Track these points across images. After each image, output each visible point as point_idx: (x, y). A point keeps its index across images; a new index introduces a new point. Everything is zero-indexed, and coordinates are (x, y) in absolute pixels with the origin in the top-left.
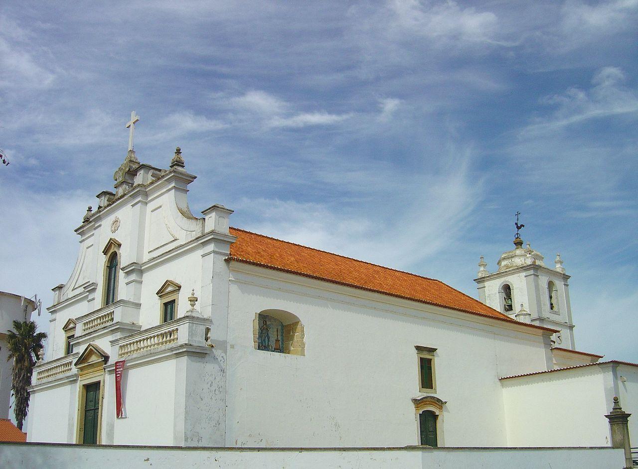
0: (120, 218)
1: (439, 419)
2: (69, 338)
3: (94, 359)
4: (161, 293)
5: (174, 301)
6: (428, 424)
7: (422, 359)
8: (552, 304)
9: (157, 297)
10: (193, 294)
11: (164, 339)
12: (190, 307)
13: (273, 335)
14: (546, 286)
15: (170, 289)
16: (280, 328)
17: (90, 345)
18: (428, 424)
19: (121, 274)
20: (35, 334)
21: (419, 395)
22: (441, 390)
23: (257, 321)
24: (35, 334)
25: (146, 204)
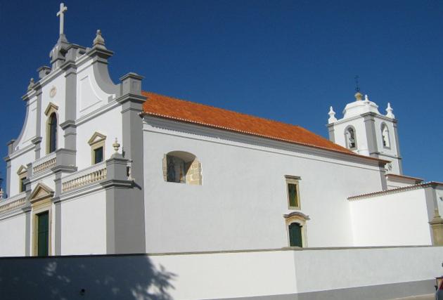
0: (57, 88)
1: (302, 229)
2: (23, 179)
3: (42, 194)
4: (91, 143)
5: (102, 148)
6: (296, 236)
7: (289, 185)
8: (384, 142)
9: (88, 145)
10: (116, 142)
11: (96, 176)
12: (115, 152)
13: (178, 169)
14: (380, 127)
15: (98, 138)
16: (182, 165)
17: (39, 184)
18: (296, 236)
19: (59, 129)
20: (389, 104)
21: (289, 212)
22: (304, 207)
23: (165, 159)
24: (389, 104)
25: (40, 87)
